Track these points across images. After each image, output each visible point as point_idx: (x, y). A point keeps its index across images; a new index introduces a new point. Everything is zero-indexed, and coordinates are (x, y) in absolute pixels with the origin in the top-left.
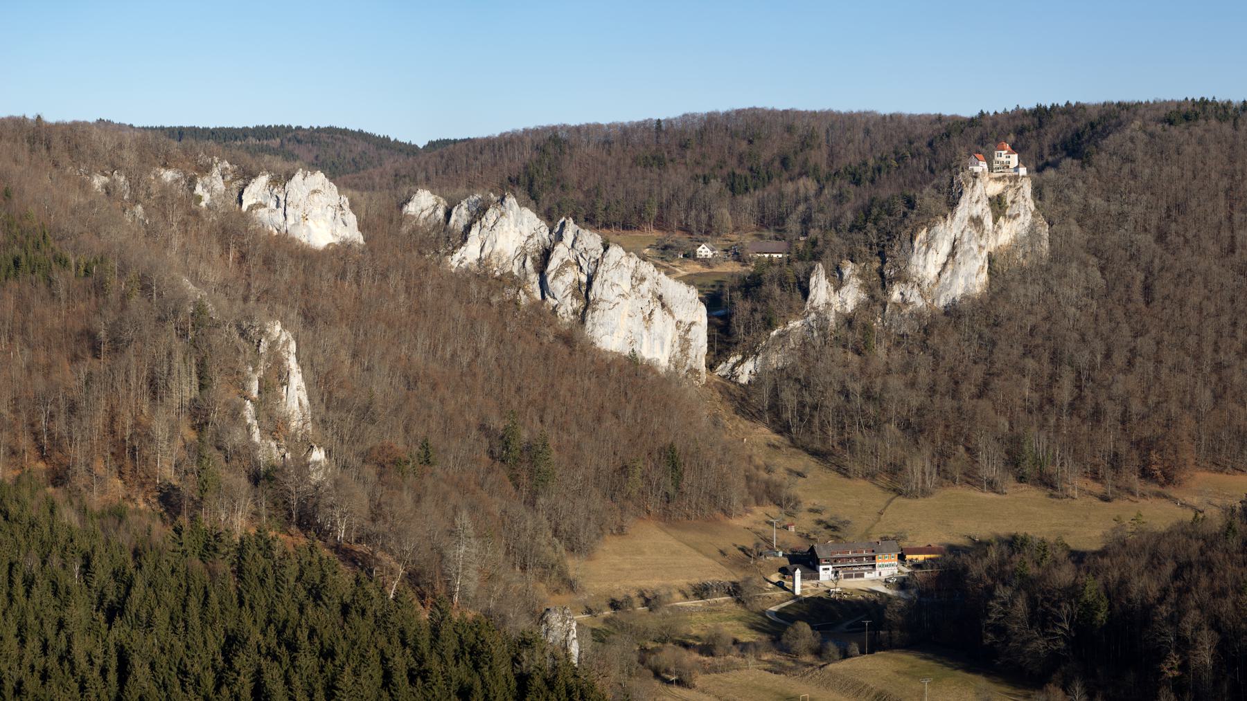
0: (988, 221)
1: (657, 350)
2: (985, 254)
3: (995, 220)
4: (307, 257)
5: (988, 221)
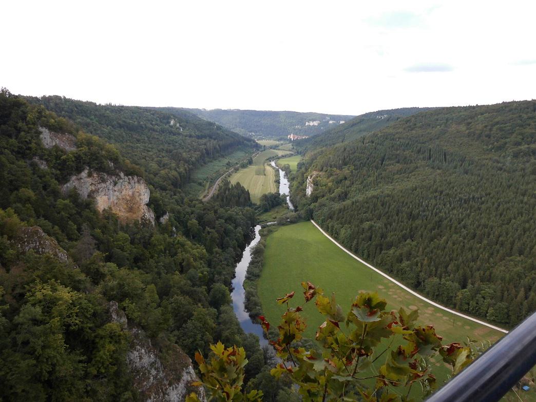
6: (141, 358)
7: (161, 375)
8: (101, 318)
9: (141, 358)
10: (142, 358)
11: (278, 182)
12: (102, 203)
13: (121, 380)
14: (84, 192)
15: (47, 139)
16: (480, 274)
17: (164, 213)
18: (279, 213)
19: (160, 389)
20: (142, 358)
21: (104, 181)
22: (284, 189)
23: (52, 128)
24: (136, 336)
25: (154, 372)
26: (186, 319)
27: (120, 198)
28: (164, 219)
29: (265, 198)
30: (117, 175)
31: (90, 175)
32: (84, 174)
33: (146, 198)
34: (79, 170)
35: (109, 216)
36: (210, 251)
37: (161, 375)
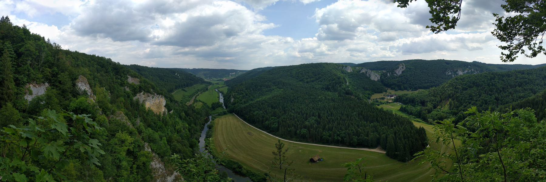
1: (376, 80)
4: (348, 73)
6: (156, 165)
7: (164, 171)
8: (141, 148)
9: (156, 165)
10: (156, 164)
11: (219, 97)
12: (148, 105)
13: (143, 170)
14: (141, 101)
15: (130, 80)
16: (31, 93)
17: (171, 110)
18: (220, 110)
19: (164, 176)
20: (156, 164)
21: (149, 96)
22: (222, 101)
23: (132, 76)
24: (154, 156)
25: (161, 170)
26: (50, 107)
27: (155, 104)
28: (172, 112)
29: (213, 104)
30: (154, 94)
31: (144, 94)
32: (142, 93)
33: (164, 104)
34: (140, 92)
35: (150, 111)
36: (189, 125)
37: (164, 171)
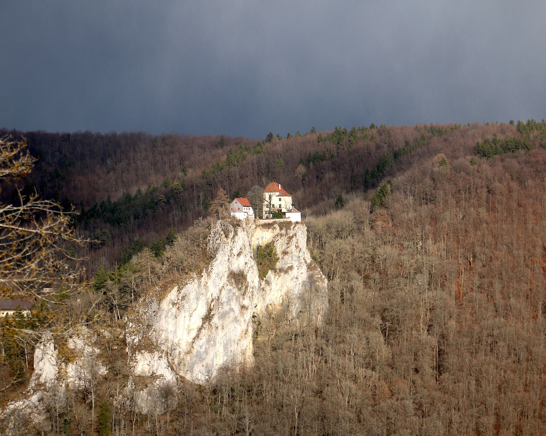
0: (253, 277)
2: (248, 315)
3: (262, 275)
5: (253, 277)
